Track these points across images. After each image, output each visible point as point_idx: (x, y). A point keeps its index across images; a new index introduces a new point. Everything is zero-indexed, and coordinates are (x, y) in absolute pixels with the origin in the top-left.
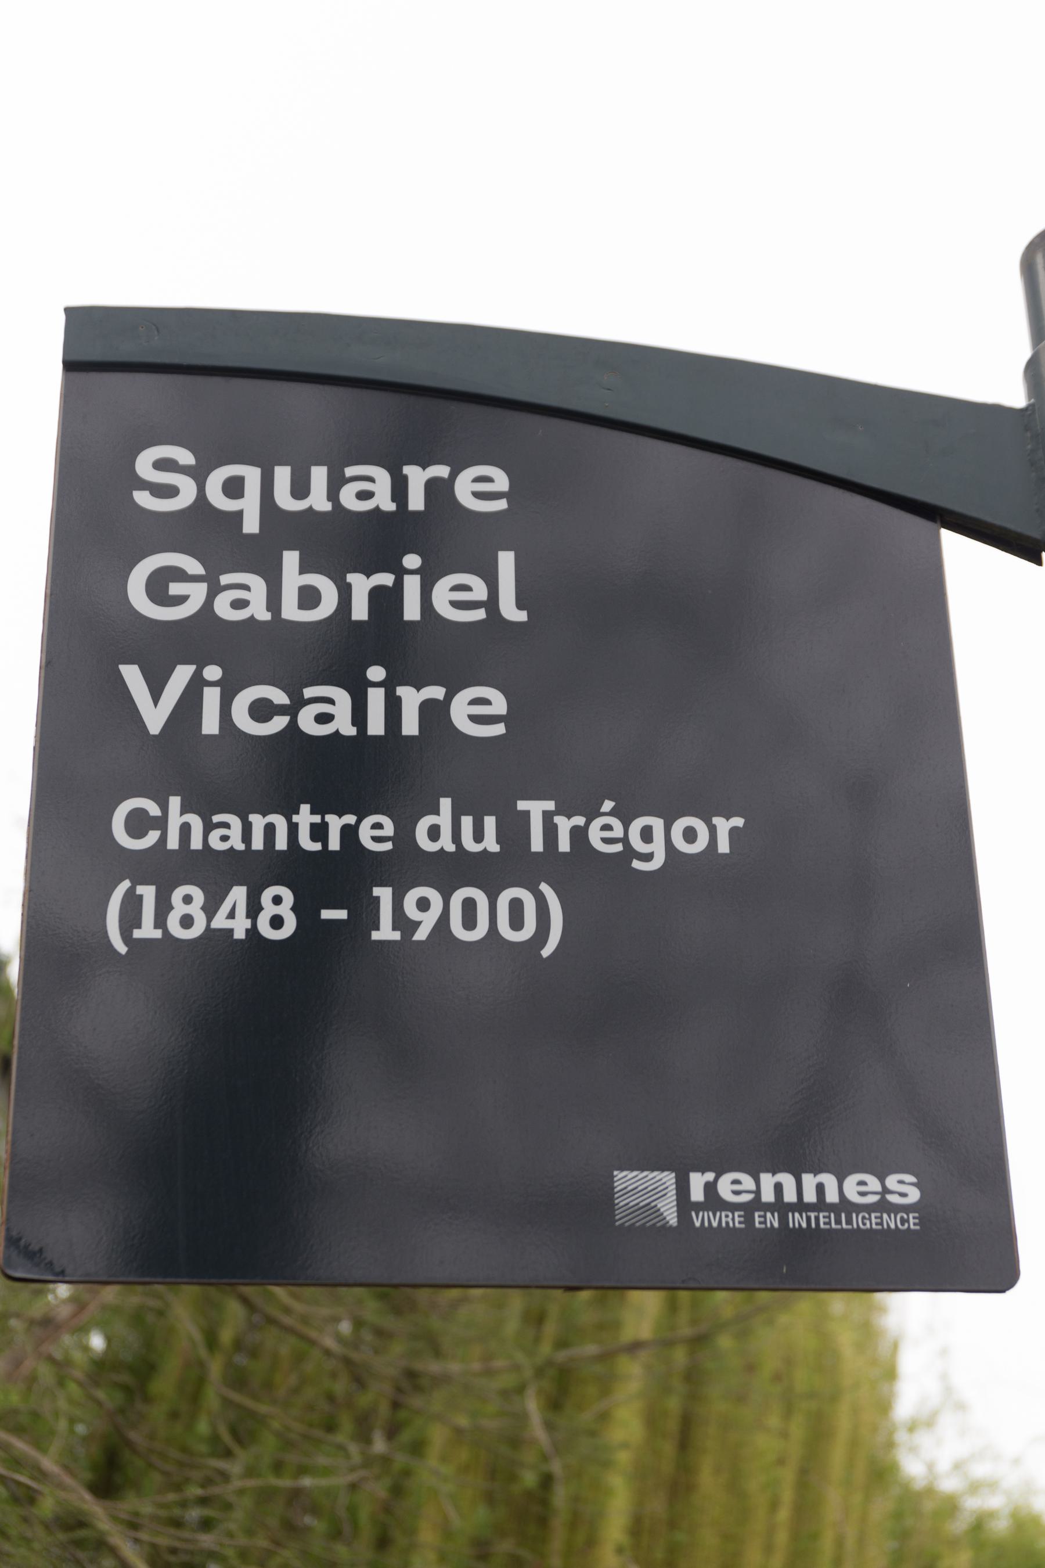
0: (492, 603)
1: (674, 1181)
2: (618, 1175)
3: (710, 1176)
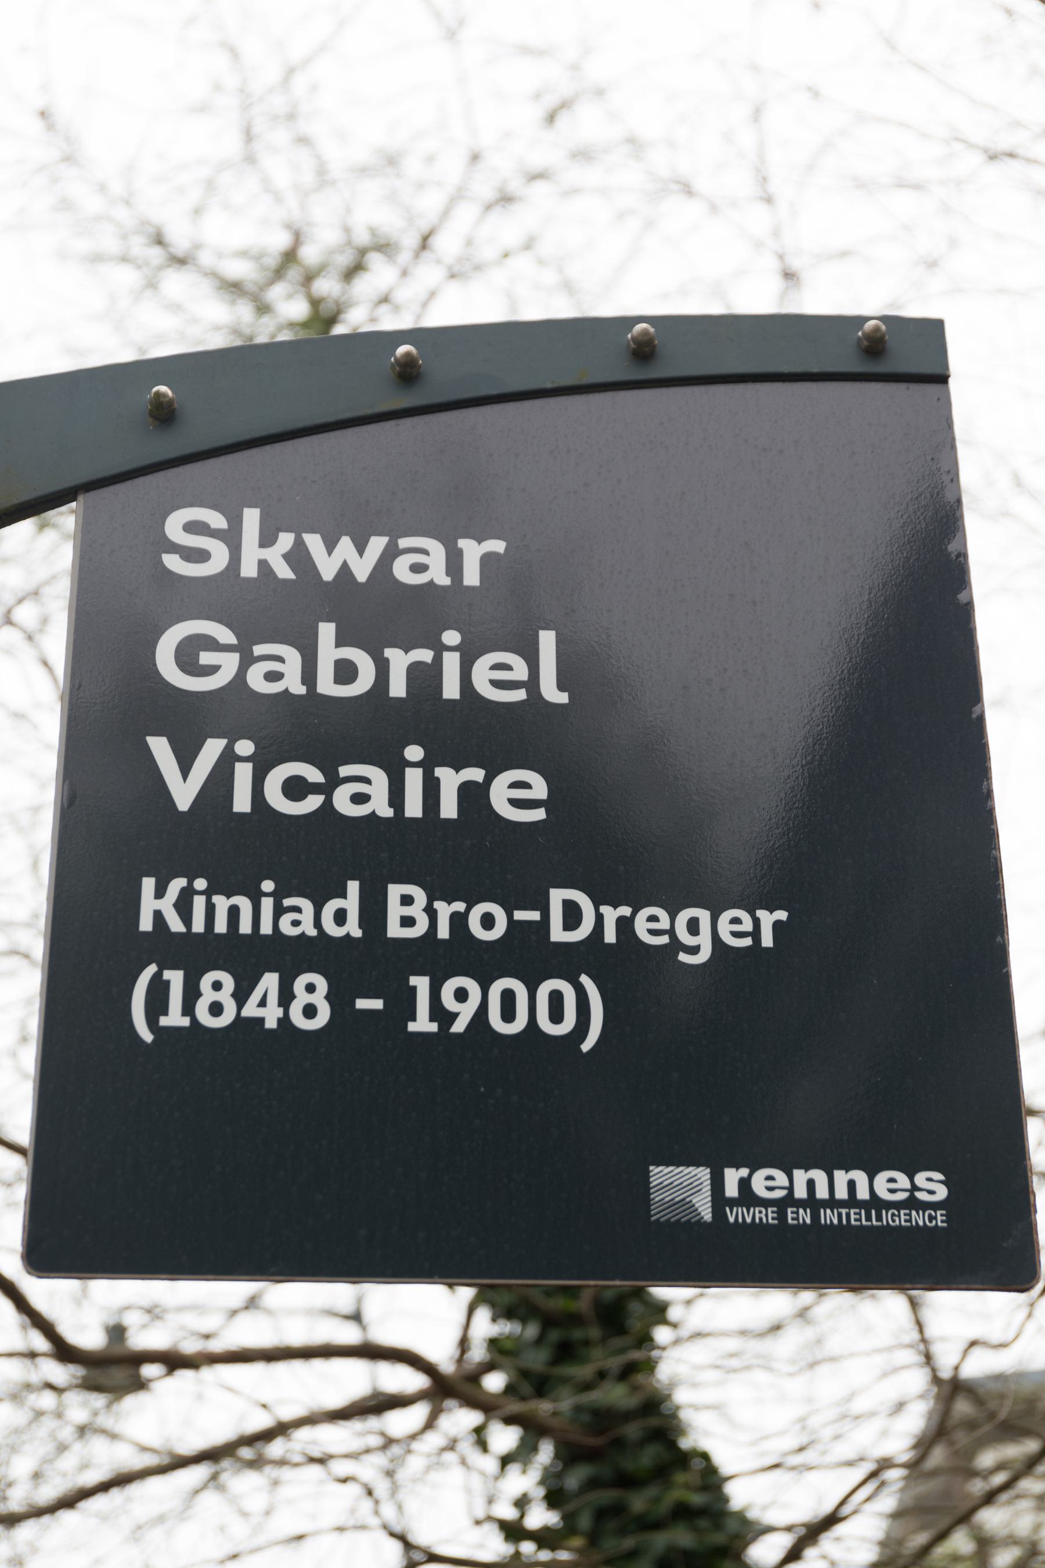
0: (532, 684)
1: (709, 1176)
2: (654, 1170)
3: (744, 1172)
